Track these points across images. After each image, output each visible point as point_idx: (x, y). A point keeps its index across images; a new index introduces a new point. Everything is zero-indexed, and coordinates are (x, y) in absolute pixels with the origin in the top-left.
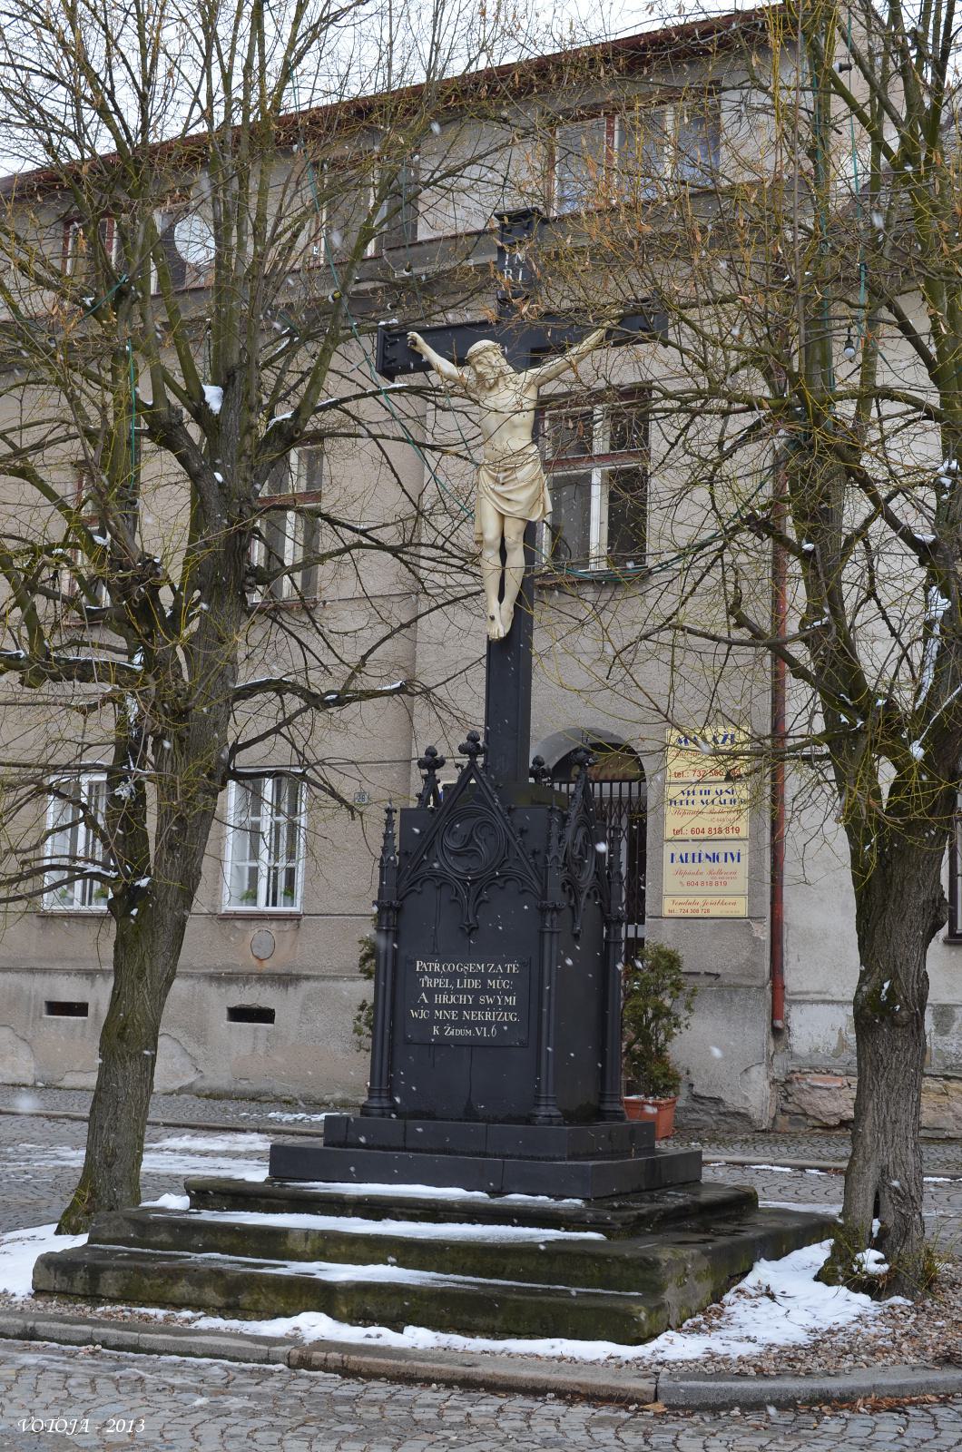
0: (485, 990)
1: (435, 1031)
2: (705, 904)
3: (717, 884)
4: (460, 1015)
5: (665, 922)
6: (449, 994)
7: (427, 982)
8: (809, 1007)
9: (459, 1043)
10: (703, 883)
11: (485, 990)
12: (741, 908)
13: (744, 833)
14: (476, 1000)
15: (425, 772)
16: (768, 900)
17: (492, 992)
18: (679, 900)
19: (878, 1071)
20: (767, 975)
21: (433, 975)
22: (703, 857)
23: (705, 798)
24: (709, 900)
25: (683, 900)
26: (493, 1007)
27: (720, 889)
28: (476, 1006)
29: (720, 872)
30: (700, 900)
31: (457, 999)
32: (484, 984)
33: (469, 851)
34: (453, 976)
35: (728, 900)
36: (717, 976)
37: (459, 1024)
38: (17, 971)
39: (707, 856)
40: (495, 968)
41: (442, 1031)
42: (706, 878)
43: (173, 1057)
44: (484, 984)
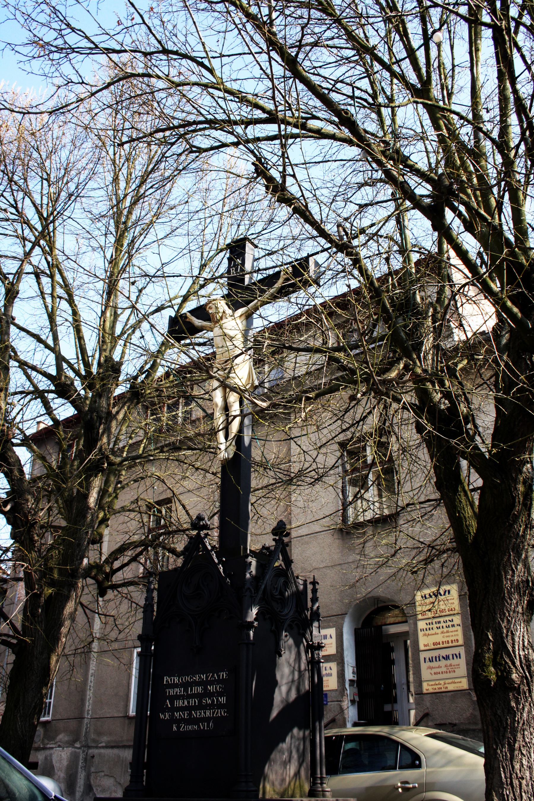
0: (207, 694)
1: (175, 728)
2: (445, 684)
3: (450, 672)
4: (190, 714)
5: (426, 696)
7: (172, 692)
10: (442, 673)
11: (207, 694)
13: (461, 642)
14: (200, 702)
17: (210, 695)
18: (431, 683)
22: (441, 658)
23: (438, 625)
24: (447, 681)
25: (433, 683)
26: (211, 706)
27: (452, 675)
28: (201, 707)
29: (451, 665)
30: (442, 682)
31: (188, 702)
32: (205, 689)
34: (186, 685)
35: (456, 680)
37: (192, 721)
38: (117, 747)
39: (443, 657)
40: (213, 676)
41: (178, 727)
42: (444, 669)
44: (205, 689)
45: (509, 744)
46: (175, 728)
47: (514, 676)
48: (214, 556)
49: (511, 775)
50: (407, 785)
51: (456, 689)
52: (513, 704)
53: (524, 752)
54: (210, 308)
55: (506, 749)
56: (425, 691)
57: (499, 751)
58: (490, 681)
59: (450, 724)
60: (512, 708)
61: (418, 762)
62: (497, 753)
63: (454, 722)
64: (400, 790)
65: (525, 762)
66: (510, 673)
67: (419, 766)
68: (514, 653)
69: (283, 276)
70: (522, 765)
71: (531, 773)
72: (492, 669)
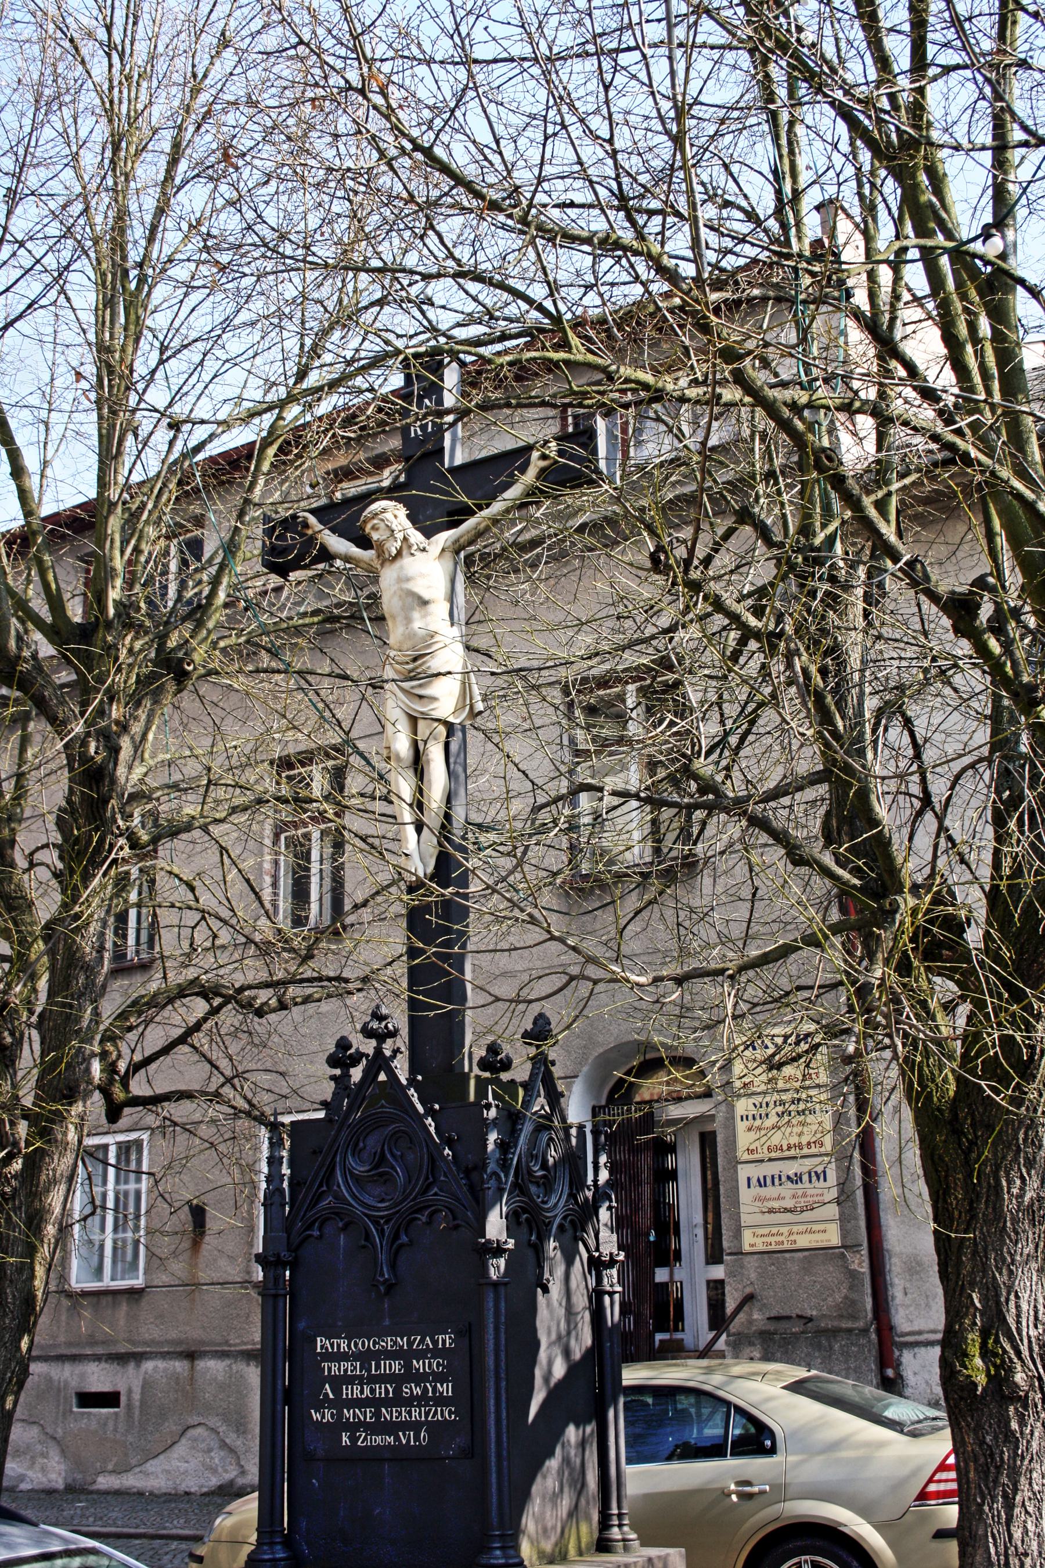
0: (410, 1376)
1: (345, 1439)
2: (791, 1233)
4: (377, 1414)
5: (748, 1258)
6: (361, 1384)
7: (335, 1369)
8: (923, 1350)
9: (374, 1455)
11: (410, 1376)
12: (832, 1237)
14: (398, 1391)
15: (338, 1072)
16: (863, 1223)
17: (419, 1378)
19: (987, 1472)
20: (870, 1315)
21: (340, 1357)
24: (795, 1229)
25: (765, 1231)
26: (422, 1400)
28: (399, 1400)
30: (785, 1230)
31: (373, 1391)
32: (408, 1366)
33: (381, 1175)
34: (365, 1357)
35: (816, 1227)
36: (810, 1319)
37: (380, 1427)
40: (422, 1341)
41: (354, 1439)
42: (789, 1204)
43: (210, 1450)
44: (408, 1366)
45: (1005, 1496)
46: (345, 1439)
47: (1019, 1377)
48: (415, 1100)
49: (1006, 1549)
50: (748, 1489)
51: (814, 1245)
52: (1014, 1425)
53: (1030, 1509)
54: (374, 528)
55: (999, 1505)
56: (746, 1248)
57: (986, 1508)
58: (975, 1385)
59: (799, 1317)
60: (1013, 1433)
61: (768, 1443)
62: (981, 1512)
63: (809, 1313)
64: (734, 1498)
65: (1031, 1527)
66: (1011, 1371)
67: (772, 1451)
68: (1020, 1334)
69: (536, 463)
70: (1026, 1531)
71: (1040, 1545)
72: (978, 1362)
